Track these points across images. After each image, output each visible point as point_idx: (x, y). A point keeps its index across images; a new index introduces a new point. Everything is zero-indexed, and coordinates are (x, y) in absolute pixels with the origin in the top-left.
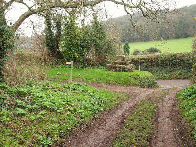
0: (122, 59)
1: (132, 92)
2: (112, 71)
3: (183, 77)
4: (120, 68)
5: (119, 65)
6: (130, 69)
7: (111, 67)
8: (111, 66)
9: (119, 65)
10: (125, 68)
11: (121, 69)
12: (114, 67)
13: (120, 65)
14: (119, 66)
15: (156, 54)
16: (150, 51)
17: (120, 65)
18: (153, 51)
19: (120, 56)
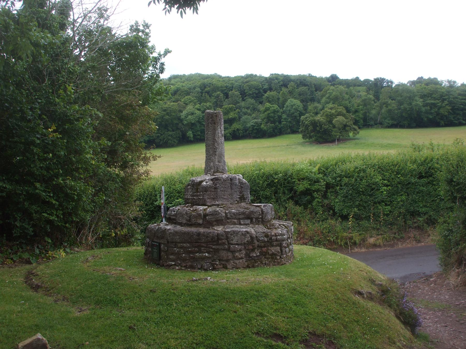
4: (251, 243)
11: (253, 250)
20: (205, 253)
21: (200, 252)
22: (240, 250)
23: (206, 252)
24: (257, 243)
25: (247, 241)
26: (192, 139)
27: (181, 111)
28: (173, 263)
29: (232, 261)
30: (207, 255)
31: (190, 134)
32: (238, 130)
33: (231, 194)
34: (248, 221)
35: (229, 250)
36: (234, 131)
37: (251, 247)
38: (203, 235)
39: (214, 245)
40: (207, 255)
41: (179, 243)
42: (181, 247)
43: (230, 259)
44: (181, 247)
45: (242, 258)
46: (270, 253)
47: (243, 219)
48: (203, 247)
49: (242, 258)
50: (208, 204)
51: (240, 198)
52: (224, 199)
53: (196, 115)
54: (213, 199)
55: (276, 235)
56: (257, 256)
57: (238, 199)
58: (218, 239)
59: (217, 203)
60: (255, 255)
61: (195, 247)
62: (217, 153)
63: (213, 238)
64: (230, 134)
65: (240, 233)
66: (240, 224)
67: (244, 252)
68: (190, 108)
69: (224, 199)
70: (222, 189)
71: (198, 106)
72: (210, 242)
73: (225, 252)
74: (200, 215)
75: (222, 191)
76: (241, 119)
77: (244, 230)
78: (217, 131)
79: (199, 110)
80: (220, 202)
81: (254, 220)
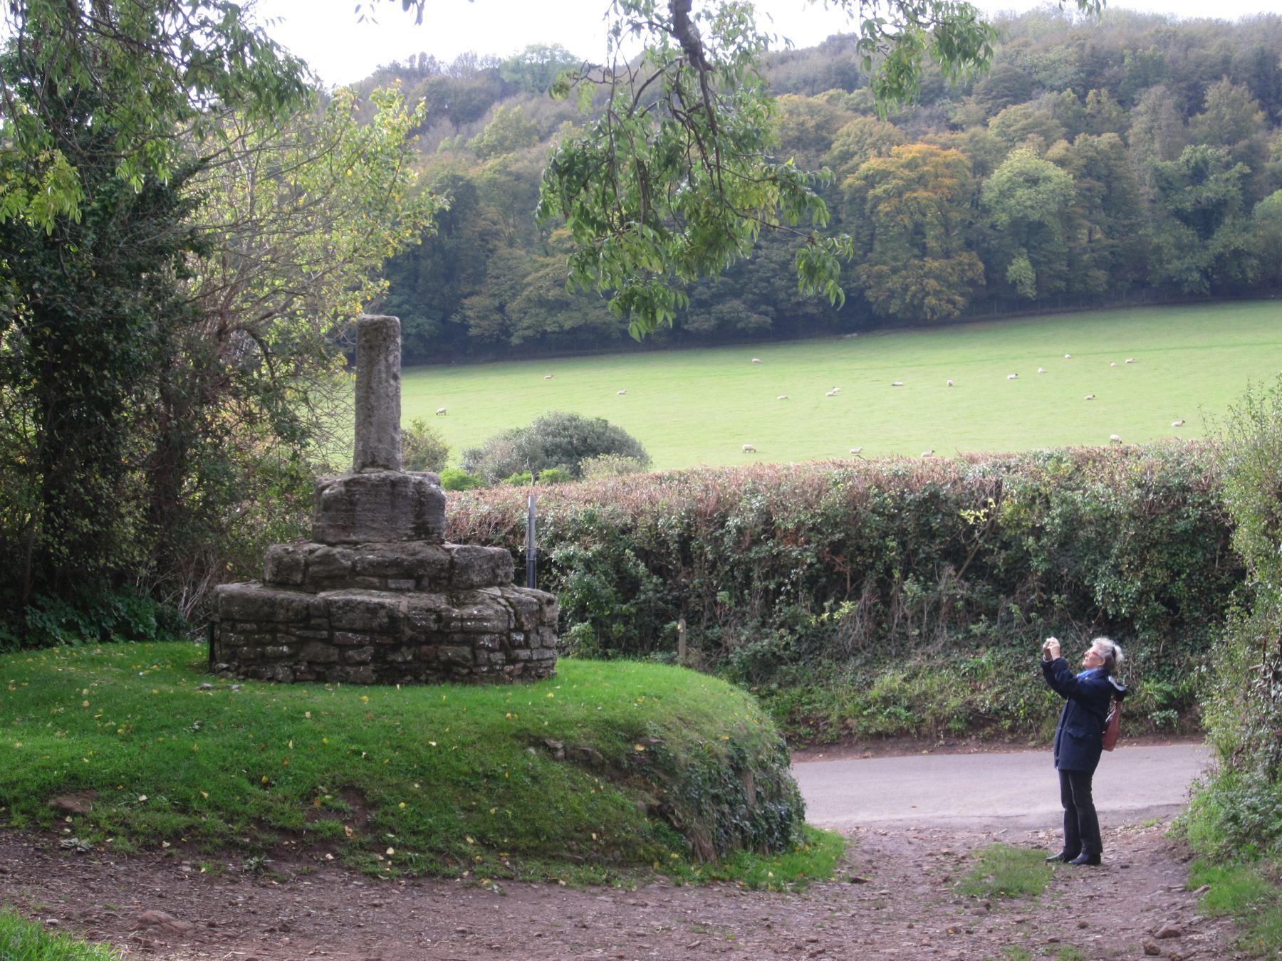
0: (406, 524)
1: (876, 818)
2: (281, 671)
3: (637, 327)
4: (391, 629)
5: (374, 598)
6: (507, 647)
7: (263, 618)
8: (271, 603)
9: (374, 598)
10: (443, 631)
11: (396, 648)
12: (306, 616)
13: (388, 599)
14: (373, 610)
15: (600, 475)
16: (548, 452)
17: (388, 599)
18: (574, 446)
19: (376, 486)
20: (282, 645)
21: (275, 643)
22: (360, 645)
23: (286, 644)
24: (409, 632)
25: (380, 625)
26: (1031, 292)
27: (982, 168)
28: (225, 666)
29: (339, 668)
30: (285, 649)
31: (1020, 268)
32: (1237, 253)
33: (392, 520)
34: (410, 583)
35: (329, 641)
36: (1219, 258)
37: (390, 641)
38: (280, 604)
39: (299, 629)
40: (285, 649)
41: (242, 621)
42: (243, 632)
43: (334, 662)
44: (243, 632)
45: (363, 663)
46: (443, 658)
47: (395, 577)
48: (280, 631)
49: (363, 663)
50: (330, 539)
51: (414, 529)
52: (373, 529)
53: (1050, 186)
54: (344, 528)
55: (462, 620)
56: (405, 662)
57: (409, 532)
58: (309, 617)
59: (354, 538)
60: (400, 659)
61: (267, 632)
62: (374, 420)
63: (297, 613)
64: (1204, 273)
65: (361, 607)
66: (387, 588)
67: (371, 650)
68: (1022, 157)
69: (373, 529)
70: (368, 506)
71: (1059, 148)
72: (292, 622)
73: (320, 645)
74: (297, 562)
75: (369, 510)
76: (1258, 206)
77: (376, 600)
78: (376, 368)
79: (1061, 162)
80: (362, 537)
81: (425, 582)
